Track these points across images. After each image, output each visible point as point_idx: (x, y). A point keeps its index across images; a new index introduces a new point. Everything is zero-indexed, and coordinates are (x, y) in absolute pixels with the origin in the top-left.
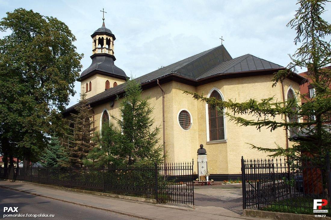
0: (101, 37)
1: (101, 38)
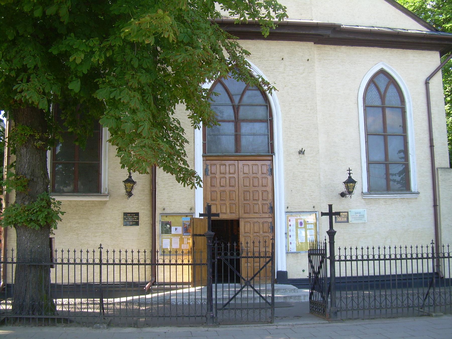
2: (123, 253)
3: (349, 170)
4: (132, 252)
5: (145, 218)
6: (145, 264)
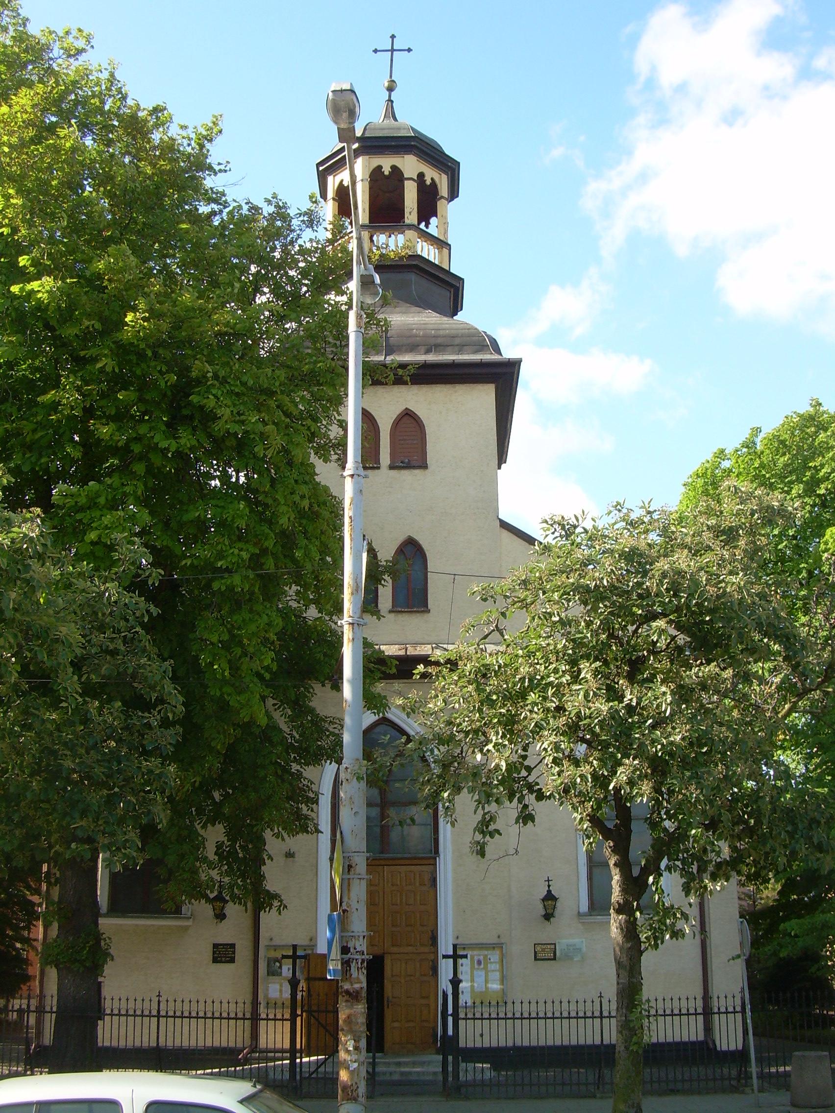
0: (386, 163)
1: (387, 170)
2: (557, 1003)
3: (548, 881)
4: (190, 1002)
5: (243, 952)
6: (244, 1019)
